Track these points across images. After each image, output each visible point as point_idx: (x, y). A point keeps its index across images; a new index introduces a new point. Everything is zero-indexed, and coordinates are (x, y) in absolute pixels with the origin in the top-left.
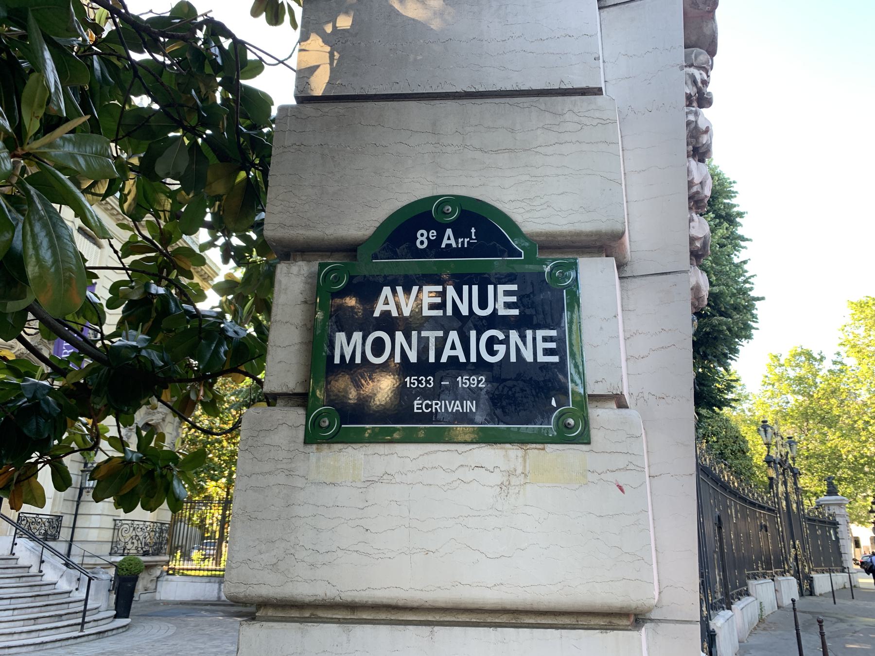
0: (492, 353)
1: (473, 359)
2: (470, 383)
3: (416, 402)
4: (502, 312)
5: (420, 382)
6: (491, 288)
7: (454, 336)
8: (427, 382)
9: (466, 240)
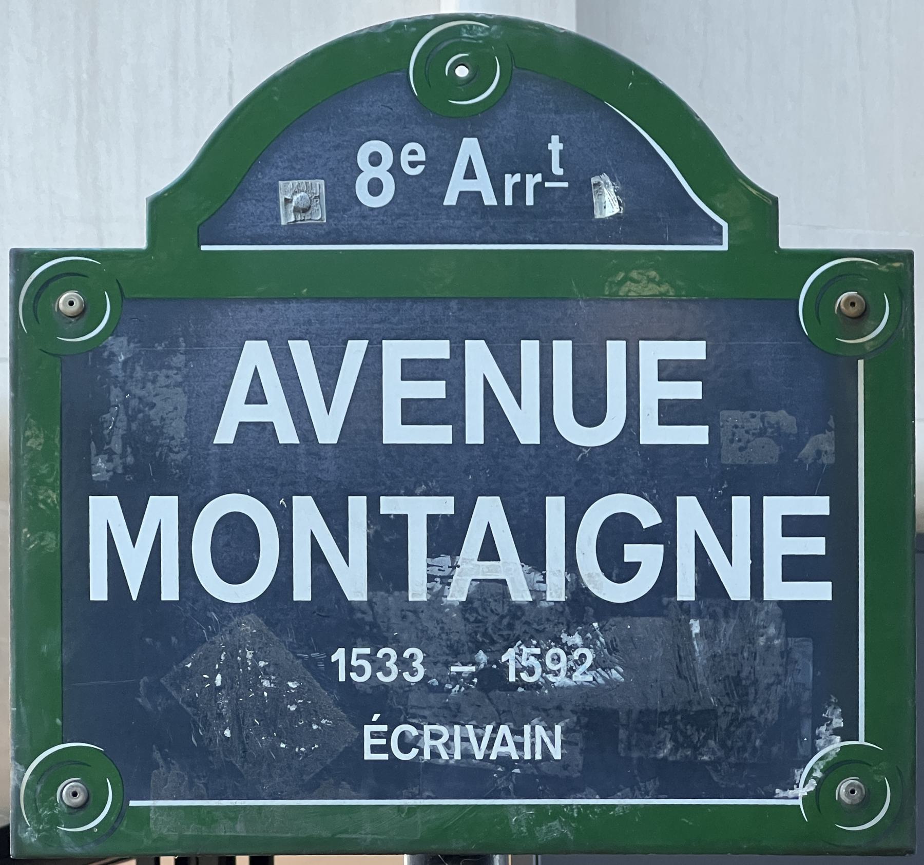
2: (545, 670)
3: (368, 729)
4: (653, 433)
5: (379, 665)
6: (616, 351)
7: (489, 512)
8: (405, 664)
9: (532, 180)
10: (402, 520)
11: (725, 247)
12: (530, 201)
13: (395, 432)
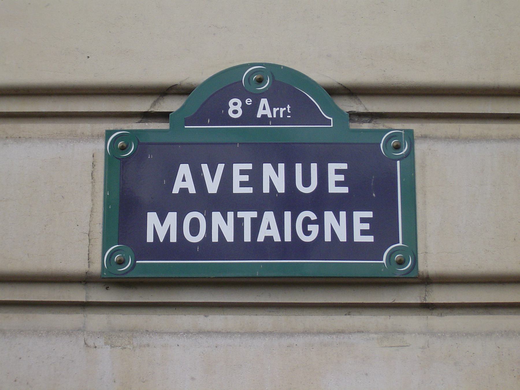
0: (307, 233)
1: (288, 238)
9: (282, 110)
10: (242, 219)
11: (332, 126)
12: (281, 116)
13: (237, 189)
